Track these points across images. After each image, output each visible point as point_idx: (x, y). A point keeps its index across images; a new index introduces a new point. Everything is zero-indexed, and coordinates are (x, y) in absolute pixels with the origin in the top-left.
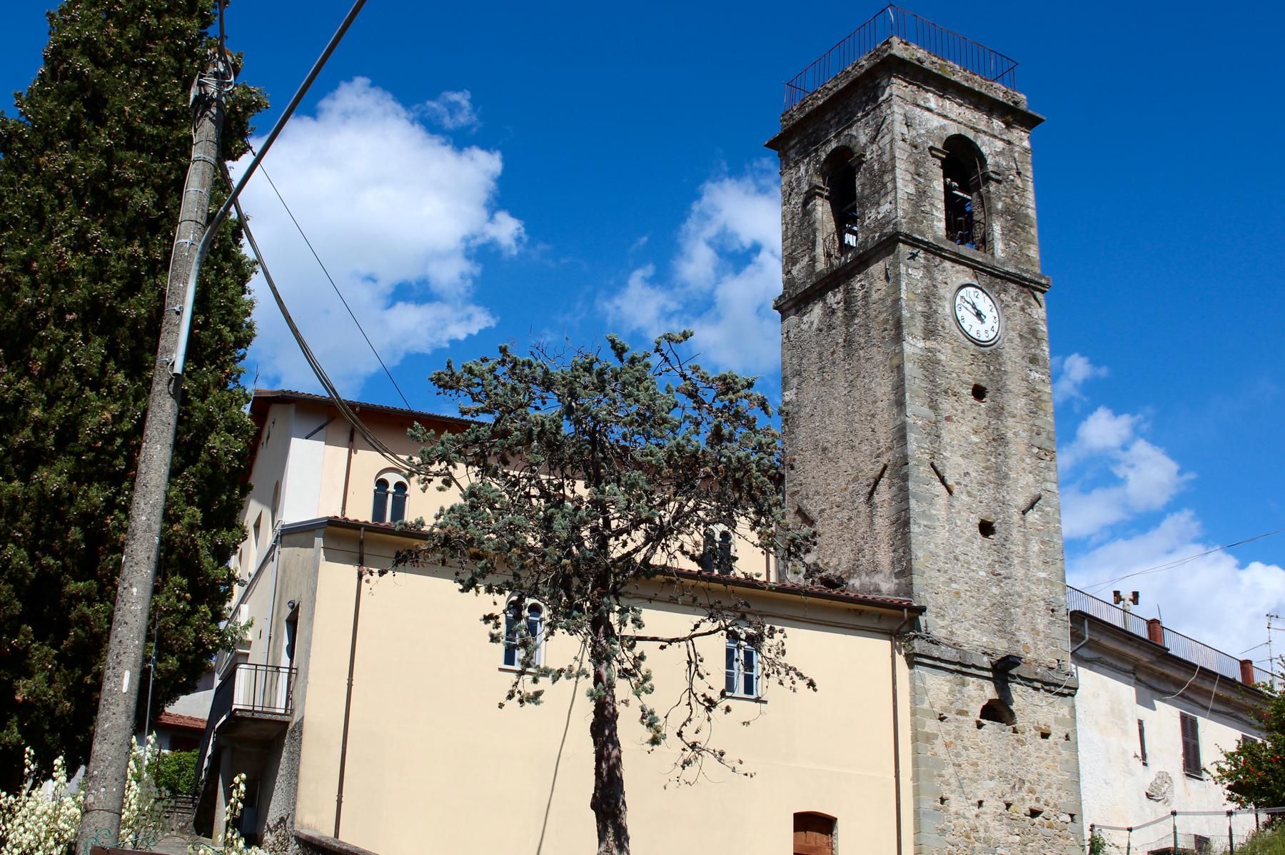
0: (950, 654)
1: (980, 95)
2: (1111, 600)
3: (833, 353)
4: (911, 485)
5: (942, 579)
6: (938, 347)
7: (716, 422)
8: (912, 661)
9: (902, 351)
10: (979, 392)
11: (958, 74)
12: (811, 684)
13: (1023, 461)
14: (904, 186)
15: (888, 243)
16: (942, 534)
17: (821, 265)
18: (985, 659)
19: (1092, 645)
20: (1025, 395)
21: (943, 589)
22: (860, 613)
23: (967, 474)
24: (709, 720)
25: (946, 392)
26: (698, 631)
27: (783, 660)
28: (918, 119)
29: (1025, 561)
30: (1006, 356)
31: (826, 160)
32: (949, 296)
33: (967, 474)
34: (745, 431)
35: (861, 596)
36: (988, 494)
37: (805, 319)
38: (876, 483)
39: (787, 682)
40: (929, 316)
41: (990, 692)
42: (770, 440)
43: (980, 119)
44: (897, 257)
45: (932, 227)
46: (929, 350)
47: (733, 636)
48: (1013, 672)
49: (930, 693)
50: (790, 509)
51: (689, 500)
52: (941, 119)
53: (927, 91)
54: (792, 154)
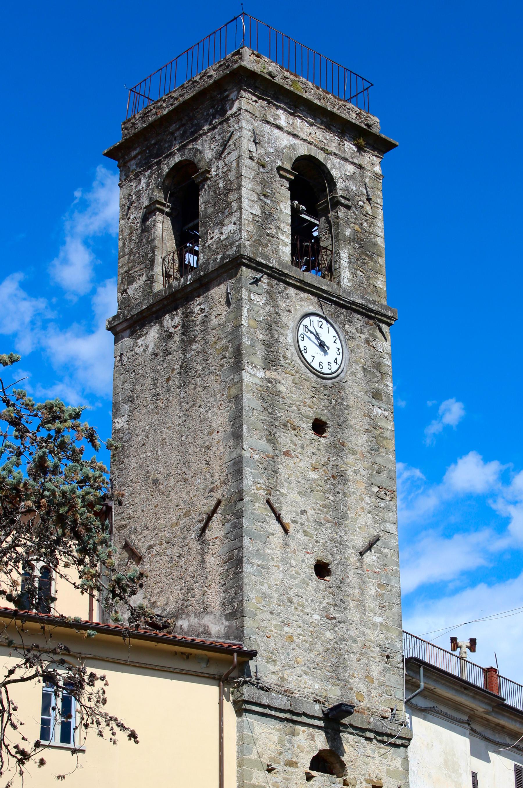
0: (280, 701)
1: (332, 115)
2: (448, 646)
3: (168, 379)
4: (245, 522)
5: (274, 622)
6: (279, 378)
7: (40, 453)
8: (240, 709)
9: (241, 381)
10: (319, 427)
11: (311, 93)
12: (133, 736)
13: (362, 500)
14: (250, 206)
15: (231, 266)
16: (276, 575)
17: (159, 286)
18: (317, 707)
19: (427, 693)
20: (367, 431)
21: (275, 632)
22: (187, 657)
23: (304, 512)
24: (21, 773)
25: (285, 426)
26: (13, 677)
27: (104, 709)
28: (265, 138)
29: (361, 605)
30: (348, 390)
31: (168, 174)
32: (292, 324)
33: (304, 512)
34: (70, 464)
35: (189, 638)
36: (325, 533)
37: (140, 342)
38: (209, 519)
39: (107, 732)
40: (270, 345)
41: (321, 742)
42: (98, 473)
43: (332, 141)
44: (239, 281)
45: (276, 251)
46: (269, 380)
47: (49, 678)
48: (346, 721)
49: (259, 743)
50: (116, 547)
51: (7, 535)
52: (291, 138)
53: (278, 108)
54: (132, 164)
